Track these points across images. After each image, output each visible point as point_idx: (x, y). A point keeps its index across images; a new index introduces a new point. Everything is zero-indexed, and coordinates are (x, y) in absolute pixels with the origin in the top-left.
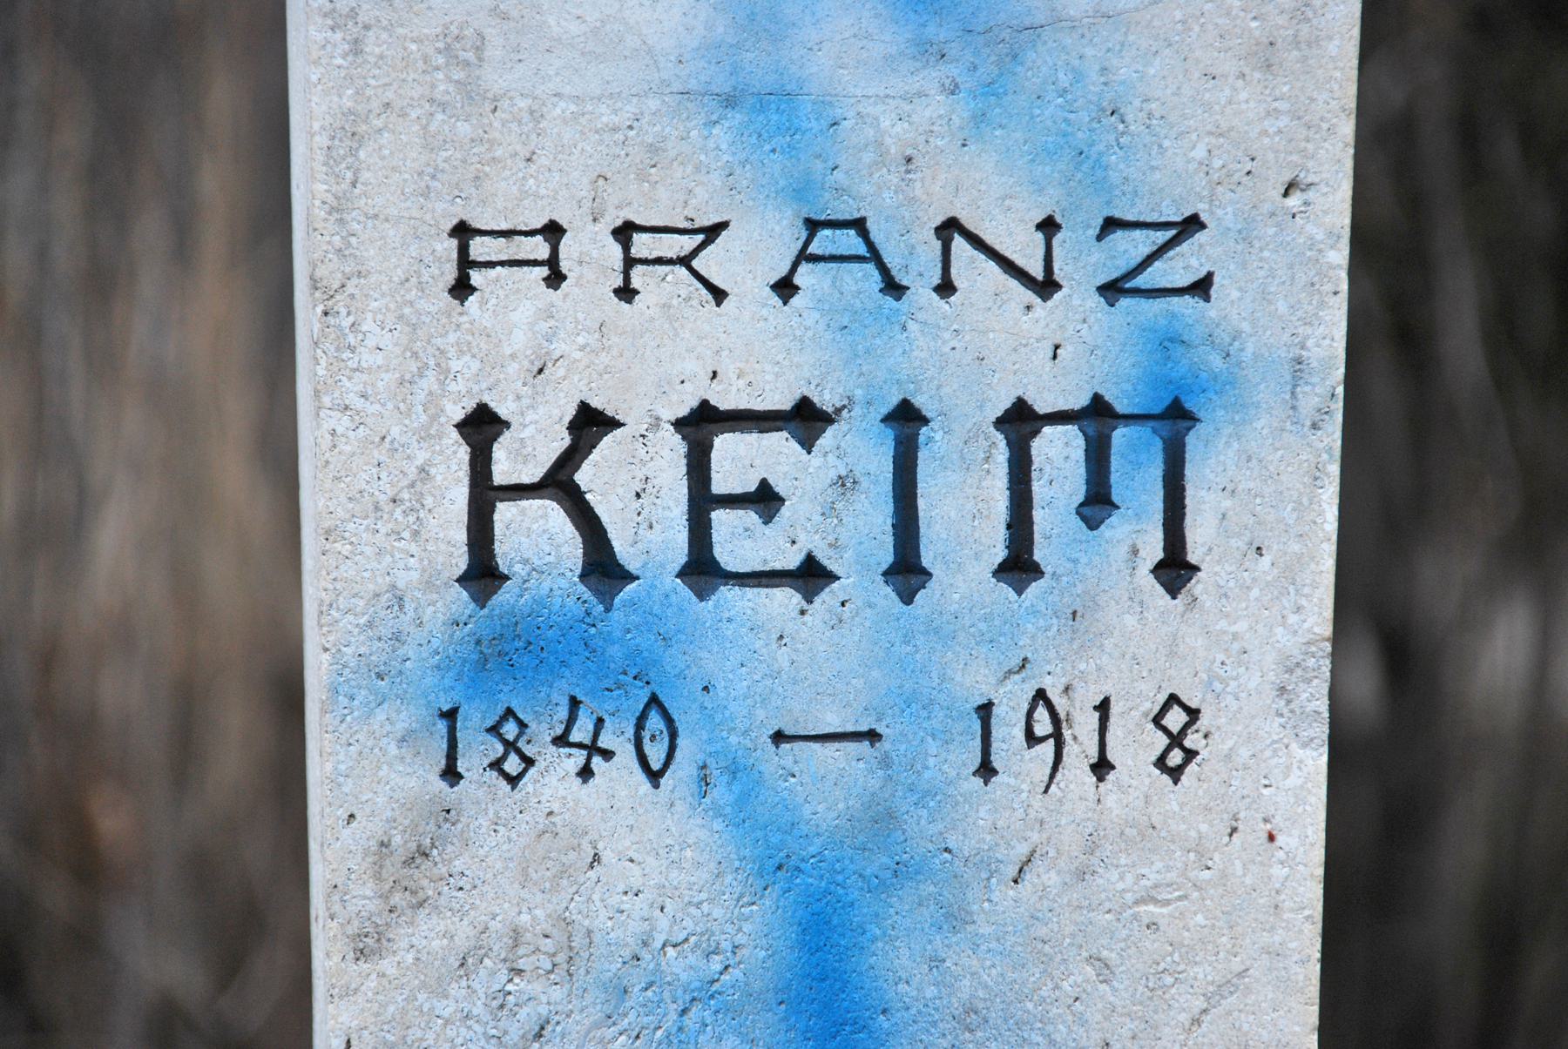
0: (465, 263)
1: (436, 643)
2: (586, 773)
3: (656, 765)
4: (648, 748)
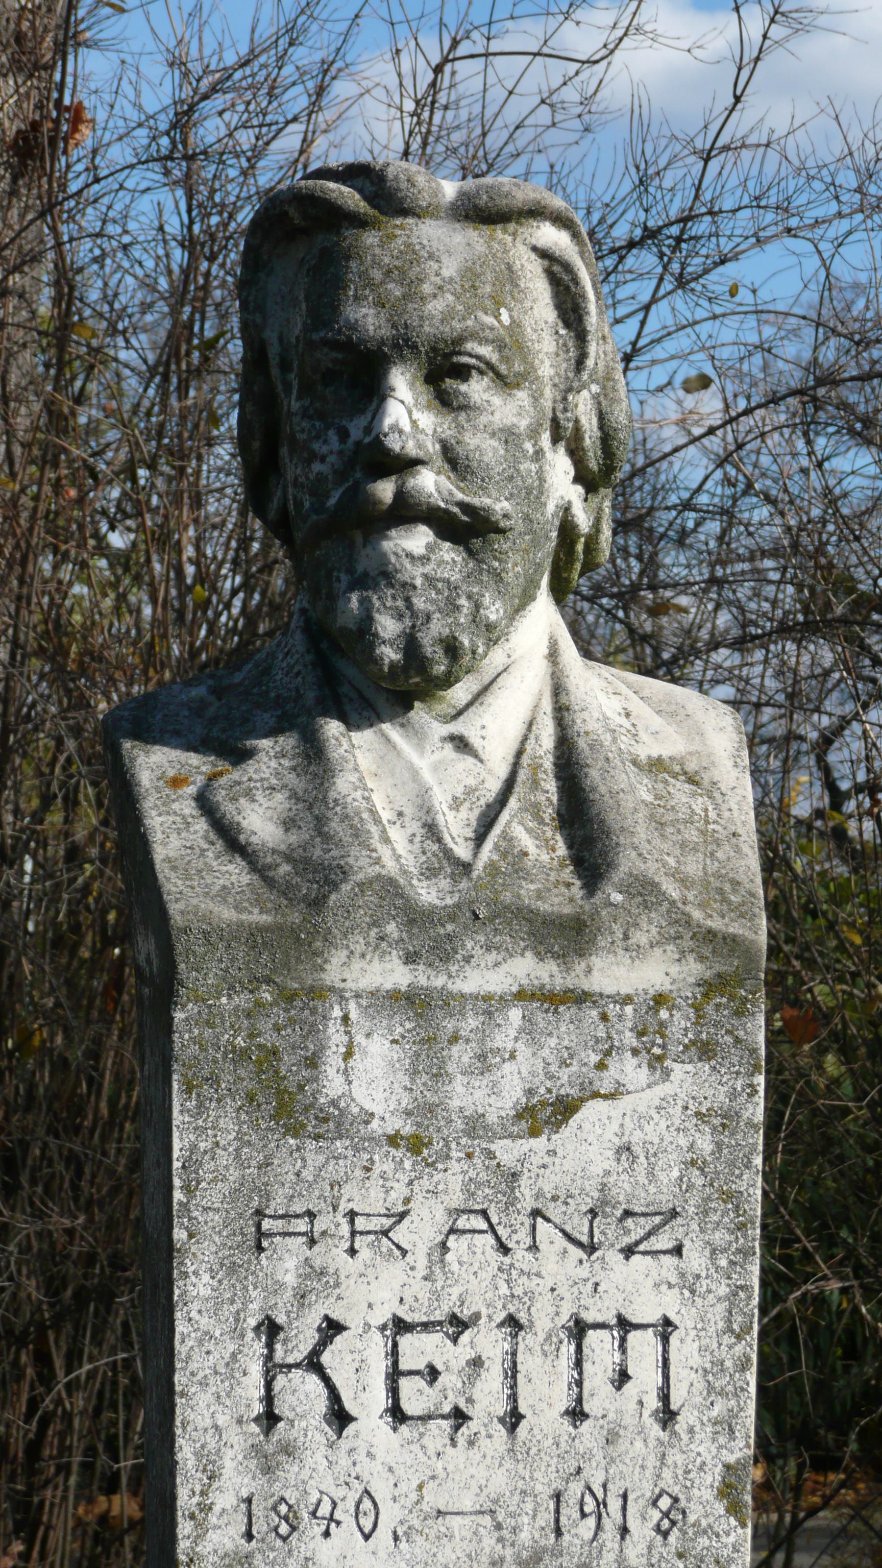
0: (260, 1234)
1: (308, 1452)
2: (327, 1534)
3: (367, 1531)
4: (362, 1521)
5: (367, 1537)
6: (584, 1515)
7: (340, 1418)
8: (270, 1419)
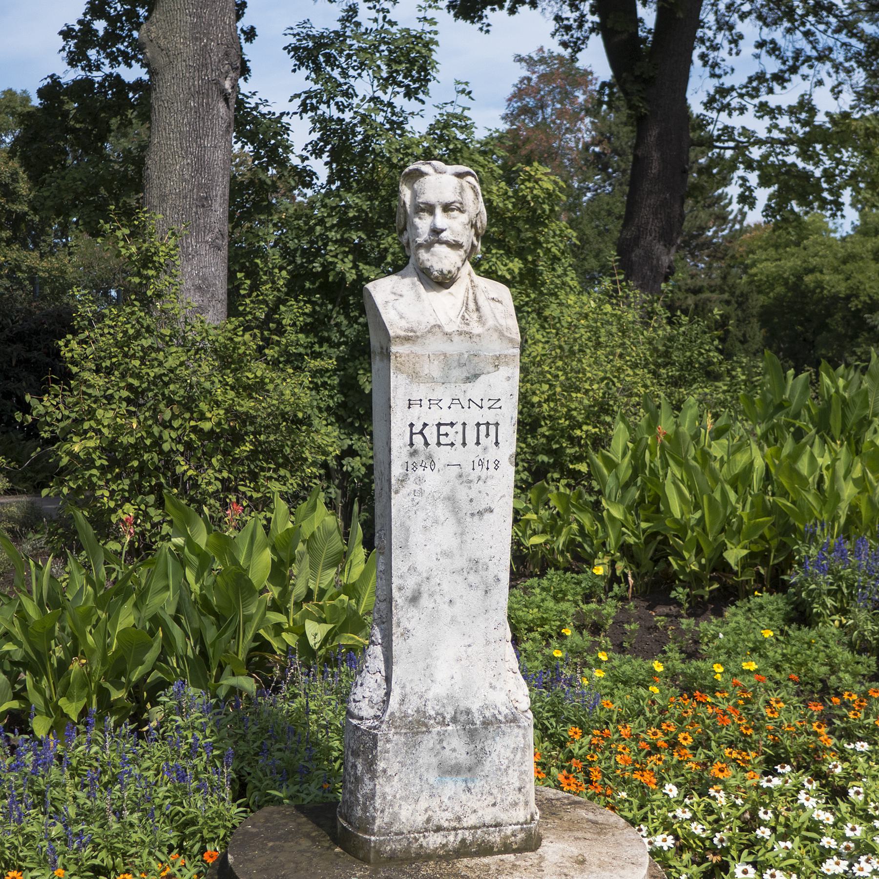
7: (427, 444)
8: (412, 444)
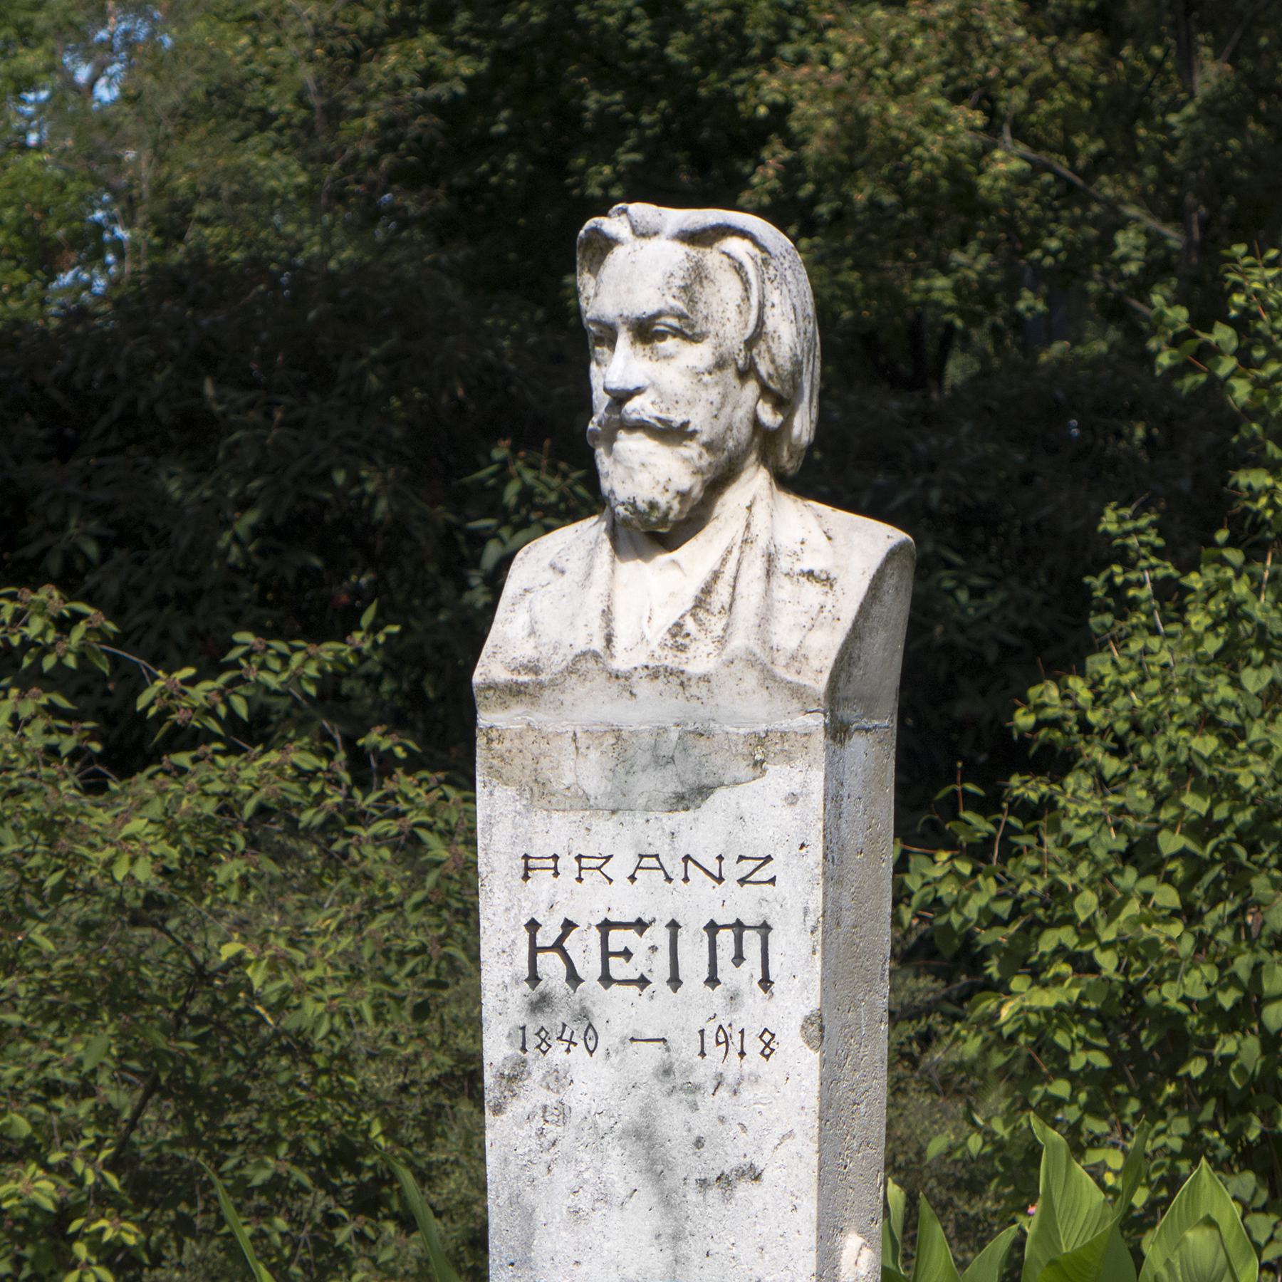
0: (527, 868)
2: (568, 1050)
5: (591, 1052)
6: (718, 1043)
7: (573, 978)
